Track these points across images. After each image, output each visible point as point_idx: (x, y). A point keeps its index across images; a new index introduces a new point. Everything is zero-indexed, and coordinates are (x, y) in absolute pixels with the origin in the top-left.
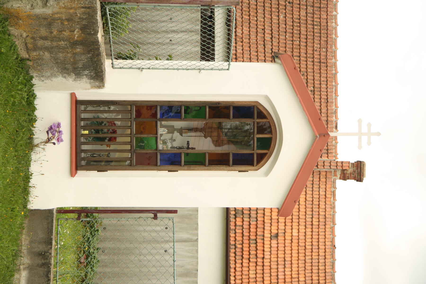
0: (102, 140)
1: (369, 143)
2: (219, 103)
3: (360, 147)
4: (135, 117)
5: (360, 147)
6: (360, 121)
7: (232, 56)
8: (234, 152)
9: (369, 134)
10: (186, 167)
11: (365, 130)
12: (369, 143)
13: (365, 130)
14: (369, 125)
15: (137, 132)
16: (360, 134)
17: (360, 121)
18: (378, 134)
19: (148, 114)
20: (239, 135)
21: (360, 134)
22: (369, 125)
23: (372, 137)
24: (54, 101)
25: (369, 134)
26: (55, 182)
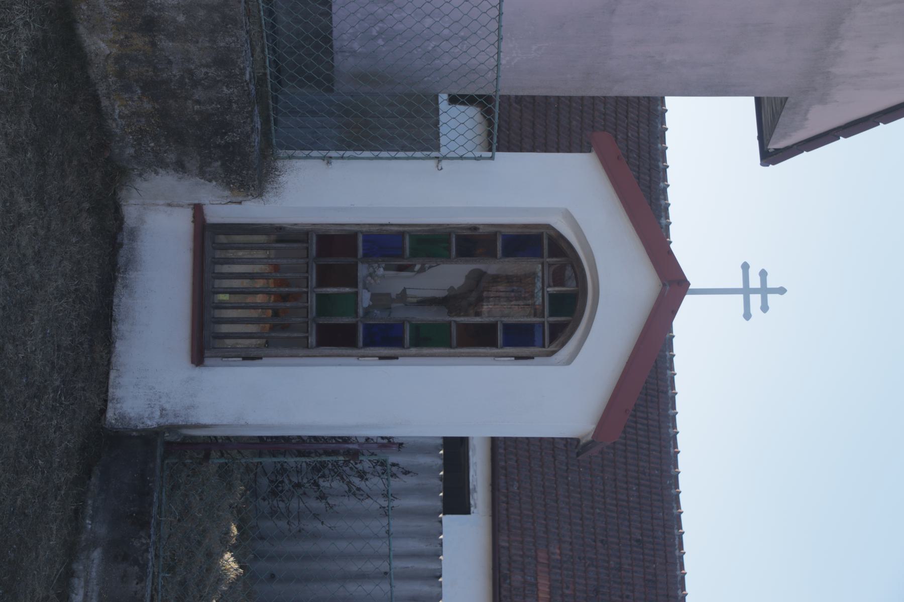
0: (284, 328)
1: (765, 308)
2: (474, 228)
3: (747, 315)
4: (314, 314)
5: (747, 315)
6: (745, 267)
7: (494, 147)
8: (506, 320)
9: (764, 291)
10: (413, 350)
11: (755, 282)
12: (765, 308)
13: (755, 282)
14: (763, 274)
15: (319, 255)
16: (746, 291)
17: (745, 267)
18: (782, 291)
19: (338, 251)
20: (521, 292)
21: (746, 291)
22: (763, 274)
23: (769, 296)
24: (162, 225)
25: (764, 291)
26: (161, 377)
